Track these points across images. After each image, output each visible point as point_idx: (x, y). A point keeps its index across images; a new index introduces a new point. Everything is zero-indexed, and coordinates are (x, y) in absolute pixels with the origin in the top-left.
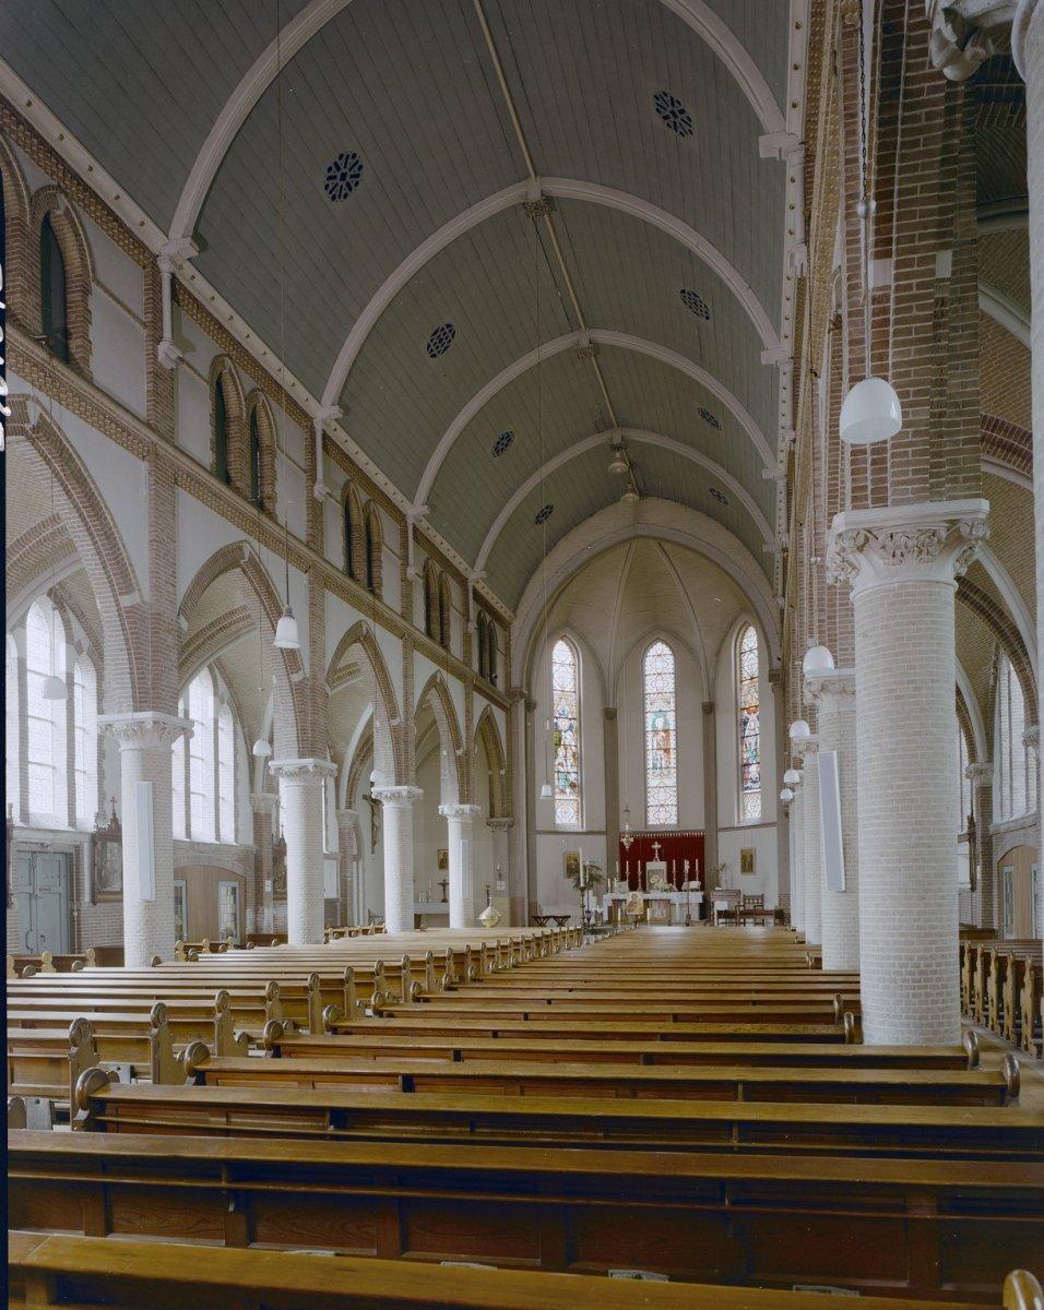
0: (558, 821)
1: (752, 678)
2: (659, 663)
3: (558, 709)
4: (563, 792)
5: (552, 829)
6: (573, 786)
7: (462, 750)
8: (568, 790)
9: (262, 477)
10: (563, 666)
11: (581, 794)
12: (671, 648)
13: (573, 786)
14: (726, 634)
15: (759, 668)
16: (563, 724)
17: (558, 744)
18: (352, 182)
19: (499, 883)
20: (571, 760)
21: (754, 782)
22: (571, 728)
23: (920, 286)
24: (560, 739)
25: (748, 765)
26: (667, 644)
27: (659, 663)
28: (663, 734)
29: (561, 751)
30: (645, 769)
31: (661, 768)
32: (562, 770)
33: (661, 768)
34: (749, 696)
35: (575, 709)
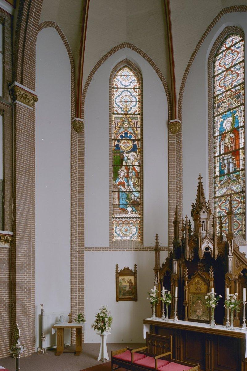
4: (124, 210)
8: (129, 209)
24: (122, 160)
28: (232, 135)
32: (123, 189)
33: (229, 173)
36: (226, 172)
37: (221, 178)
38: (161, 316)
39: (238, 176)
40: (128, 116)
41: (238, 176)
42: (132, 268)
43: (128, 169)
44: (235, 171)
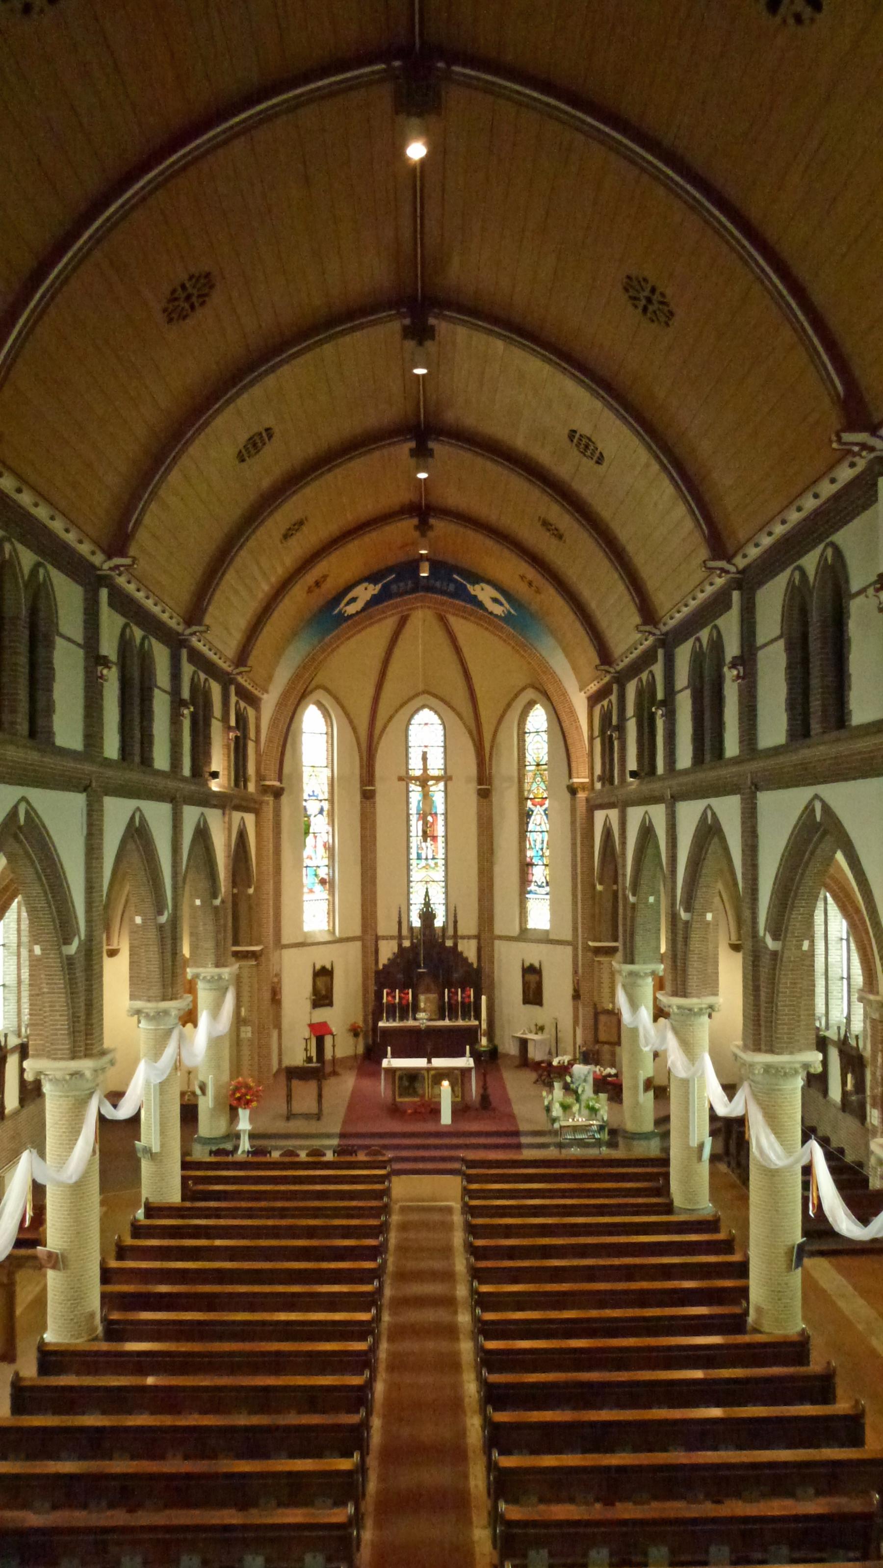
0: (307, 928)
1: (538, 765)
2: (426, 736)
3: (307, 790)
4: (311, 891)
5: (300, 940)
6: (323, 882)
7: (76, 943)
9: (513, 647)
10: (316, 738)
11: (332, 892)
12: (440, 718)
13: (323, 882)
14: (513, 707)
15: (549, 753)
16: (312, 807)
17: (307, 833)
18: (180, 293)
19: (243, 1029)
20: (321, 851)
21: (540, 887)
22: (321, 811)
23: (57, 1025)
24: (308, 826)
25: (531, 865)
26: (436, 712)
27: (426, 736)
29: (310, 840)
30: (408, 859)
31: (427, 859)
33: (427, 859)
34: (534, 786)
35: (326, 788)
36: (424, 857)
37: (419, 861)
38: (470, 1019)
39: (436, 864)
40: (540, 767)
41: (436, 864)
42: (328, 967)
43: (315, 837)
44: (434, 858)
